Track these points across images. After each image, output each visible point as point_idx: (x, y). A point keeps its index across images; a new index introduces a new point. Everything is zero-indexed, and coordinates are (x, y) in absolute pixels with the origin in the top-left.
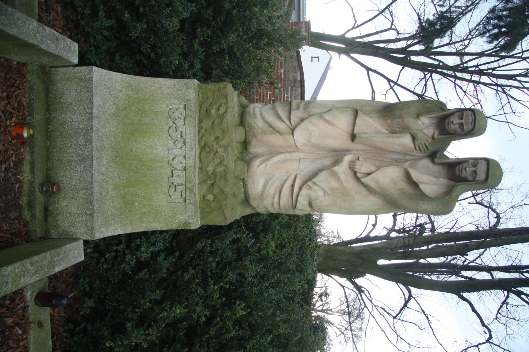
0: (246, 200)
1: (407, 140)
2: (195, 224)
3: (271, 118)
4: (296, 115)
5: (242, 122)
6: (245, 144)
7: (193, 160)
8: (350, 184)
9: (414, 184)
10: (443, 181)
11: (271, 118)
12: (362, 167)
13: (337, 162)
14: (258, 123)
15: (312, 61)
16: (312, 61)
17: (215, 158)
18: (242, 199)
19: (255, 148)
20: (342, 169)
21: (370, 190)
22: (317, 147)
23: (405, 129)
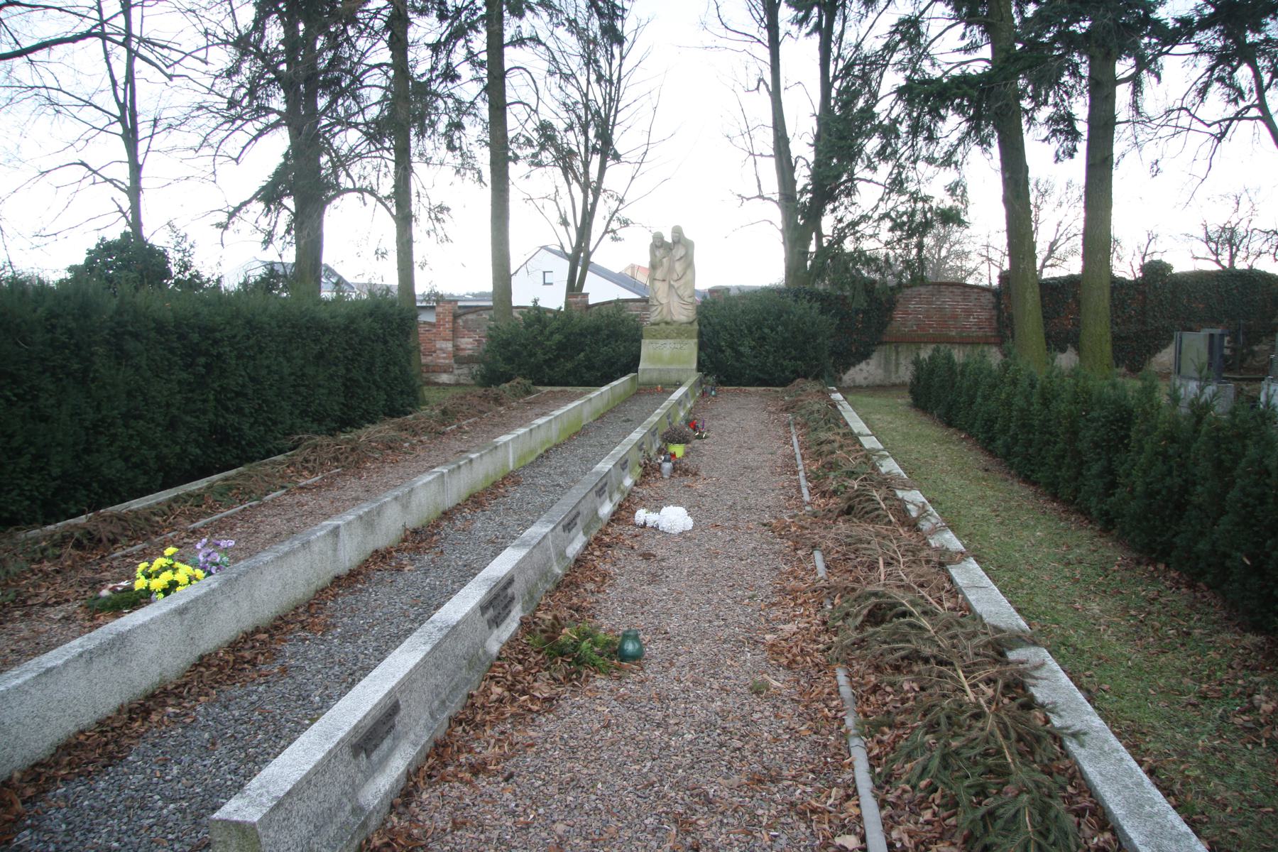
0: (691, 323)
1: (665, 260)
2: (696, 340)
3: (656, 313)
4: (656, 303)
5: (658, 324)
6: (667, 323)
7: (669, 341)
8: (682, 281)
9: (681, 258)
10: (680, 246)
11: (656, 313)
12: (675, 277)
13: (673, 286)
14: (658, 318)
15: (551, 284)
16: (551, 284)
17: (1051, 716)
18: (1080, 528)
19: (668, 319)
20: (676, 285)
21: (684, 274)
22: (668, 295)
23: (661, 261)
